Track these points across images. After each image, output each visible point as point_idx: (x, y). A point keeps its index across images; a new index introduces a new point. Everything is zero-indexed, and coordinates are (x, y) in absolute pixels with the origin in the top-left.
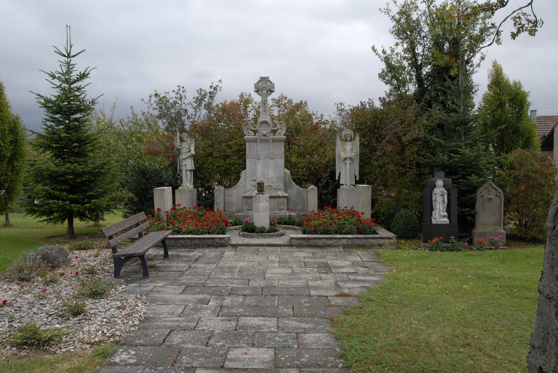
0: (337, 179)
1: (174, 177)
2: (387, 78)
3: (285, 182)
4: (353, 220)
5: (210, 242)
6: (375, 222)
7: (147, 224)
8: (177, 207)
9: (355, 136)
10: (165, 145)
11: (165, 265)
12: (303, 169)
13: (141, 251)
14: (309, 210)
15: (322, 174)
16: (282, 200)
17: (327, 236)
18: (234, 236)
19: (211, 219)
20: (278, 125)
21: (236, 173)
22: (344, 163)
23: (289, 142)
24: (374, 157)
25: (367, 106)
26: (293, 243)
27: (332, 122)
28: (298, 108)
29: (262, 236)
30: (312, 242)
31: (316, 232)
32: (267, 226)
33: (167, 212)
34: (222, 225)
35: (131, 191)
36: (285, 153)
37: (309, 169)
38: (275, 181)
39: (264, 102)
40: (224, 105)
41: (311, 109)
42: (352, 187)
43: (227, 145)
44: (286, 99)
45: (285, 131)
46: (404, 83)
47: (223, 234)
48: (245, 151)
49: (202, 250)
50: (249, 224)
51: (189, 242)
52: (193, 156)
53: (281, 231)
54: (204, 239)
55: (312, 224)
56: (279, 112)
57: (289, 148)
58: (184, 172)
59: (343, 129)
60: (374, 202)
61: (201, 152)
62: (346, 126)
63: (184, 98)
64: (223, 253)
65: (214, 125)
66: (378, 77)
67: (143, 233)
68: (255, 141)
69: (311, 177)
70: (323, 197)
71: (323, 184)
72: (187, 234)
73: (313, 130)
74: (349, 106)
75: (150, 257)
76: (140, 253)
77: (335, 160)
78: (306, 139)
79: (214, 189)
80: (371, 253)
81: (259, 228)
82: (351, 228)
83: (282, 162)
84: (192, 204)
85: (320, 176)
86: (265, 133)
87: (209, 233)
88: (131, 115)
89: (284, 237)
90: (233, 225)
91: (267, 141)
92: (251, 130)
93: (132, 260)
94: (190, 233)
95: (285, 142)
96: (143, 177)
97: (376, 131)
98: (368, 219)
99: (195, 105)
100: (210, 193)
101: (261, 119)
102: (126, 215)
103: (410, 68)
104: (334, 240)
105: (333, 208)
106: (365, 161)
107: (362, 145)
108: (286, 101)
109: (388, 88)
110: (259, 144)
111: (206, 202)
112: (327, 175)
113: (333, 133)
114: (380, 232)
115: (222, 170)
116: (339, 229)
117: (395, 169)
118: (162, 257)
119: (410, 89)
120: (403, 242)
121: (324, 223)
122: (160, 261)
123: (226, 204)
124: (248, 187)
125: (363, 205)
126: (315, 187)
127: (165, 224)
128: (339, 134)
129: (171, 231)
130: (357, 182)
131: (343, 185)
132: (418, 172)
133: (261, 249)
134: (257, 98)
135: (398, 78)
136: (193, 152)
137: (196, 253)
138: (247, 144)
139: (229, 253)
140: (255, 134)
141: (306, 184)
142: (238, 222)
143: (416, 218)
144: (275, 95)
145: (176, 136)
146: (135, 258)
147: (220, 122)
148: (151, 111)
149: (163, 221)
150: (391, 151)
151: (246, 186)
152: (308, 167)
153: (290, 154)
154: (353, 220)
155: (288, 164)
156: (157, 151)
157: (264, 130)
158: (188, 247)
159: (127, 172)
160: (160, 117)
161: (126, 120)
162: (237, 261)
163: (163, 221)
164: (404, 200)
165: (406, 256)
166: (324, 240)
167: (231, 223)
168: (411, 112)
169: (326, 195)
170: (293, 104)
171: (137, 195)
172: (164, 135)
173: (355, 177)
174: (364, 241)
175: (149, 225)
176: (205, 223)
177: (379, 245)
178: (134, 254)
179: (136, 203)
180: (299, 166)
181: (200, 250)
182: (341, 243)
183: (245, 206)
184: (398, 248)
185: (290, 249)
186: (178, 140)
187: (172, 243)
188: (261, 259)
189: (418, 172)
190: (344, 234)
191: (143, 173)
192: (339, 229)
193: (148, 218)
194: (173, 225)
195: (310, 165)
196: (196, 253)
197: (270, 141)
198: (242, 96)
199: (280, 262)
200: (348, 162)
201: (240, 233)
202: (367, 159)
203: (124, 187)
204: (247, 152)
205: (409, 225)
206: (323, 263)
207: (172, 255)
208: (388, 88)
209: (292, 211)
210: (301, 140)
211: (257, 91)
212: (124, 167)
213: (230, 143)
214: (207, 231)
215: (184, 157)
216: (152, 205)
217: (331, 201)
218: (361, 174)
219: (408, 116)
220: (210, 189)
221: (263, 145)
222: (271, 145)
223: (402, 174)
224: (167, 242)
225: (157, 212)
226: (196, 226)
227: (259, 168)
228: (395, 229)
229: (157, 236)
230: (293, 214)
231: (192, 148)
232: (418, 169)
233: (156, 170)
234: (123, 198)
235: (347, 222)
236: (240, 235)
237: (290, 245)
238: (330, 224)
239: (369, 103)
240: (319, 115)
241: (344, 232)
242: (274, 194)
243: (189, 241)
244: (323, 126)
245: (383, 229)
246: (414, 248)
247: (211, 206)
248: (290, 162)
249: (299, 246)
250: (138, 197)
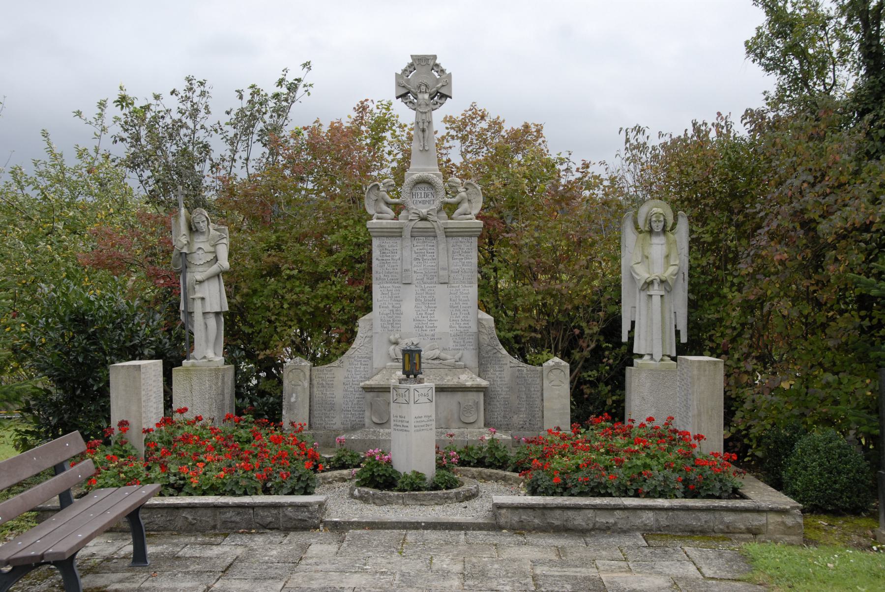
0: (625, 338)
1: (169, 331)
2: (769, 54)
3: (479, 348)
4: (672, 457)
5: (268, 517)
6: (736, 463)
7: (87, 466)
8: (177, 417)
9: (676, 218)
10: (146, 241)
11: (136, 586)
12: (530, 311)
13: (63, 547)
14: (546, 427)
15: (584, 324)
16: (472, 397)
17: (598, 501)
18: (337, 499)
19: (273, 450)
20: (461, 189)
21: (345, 323)
22: (643, 295)
23: (490, 239)
24: (730, 278)
25: (713, 135)
26: (502, 521)
27: (613, 180)
28: (519, 143)
29: (416, 499)
30: (556, 518)
31: (565, 490)
32: (429, 470)
33: (148, 431)
34: (303, 468)
35: (42, 370)
36: (480, 265)
37: (545, 310)
38: (451, 345)
39: (423, 127)
40: (314, 132)
41: (554, 146)
42: (668, 361)
43: (322, 246)
44: (483, 118)
45: (480, 205)
46: (822, 64)
47: (306, 493)
48: (370, 263)
49: (245, 539)
50: (379, 465)
51: (207, 518)
52: (224, 273)
53: (469, 485)
54: (252, 507)
55: (554, 465)
56: (463, 154)
57: (492, 253)
58: (198, 318)
59: (643, 201)
60: (731, 406)
61: (249, 264)
62: (650, 192)
63: (202, 114)
64: (305, 548)
65: (284, 188)
66: (744, 50)
67: (74, 493)
68: (396, 234)
69: (553, 332)
70: (587, 390)
71: (586, 353)
72: (204, 493)
73: (558, 202)
74: (661, 134)
75: (92, 562)
76: (63, 554)
77: (618, 287)
78: (538, 228)
79: (281, 365)
80: (728, 554)
81: (406, 476)
82: (666, 479)
83: (473, 292)
84: (221, 408)
85: (577, 331)
86: (424, 211)
87: (266, 491)
88: (46, 158)
89: (475, 503)
90: (333, 468)
91: (429, 234)
92: (388, 204)
93: (34, 573)
94: (213, 490)
95: (481, 237)
96: (79, 332)
97: (736, 205)
98: (716, 455)
99: (231, 132)
100: (270, 376)
101: (414, 173)
102: (25, 441)
103: (843, 20)
104: (618, 513)
105: (613, 421)
106: (702, 292)
107: (695, 242)
108: (484, 125)
109: (772, 82)
110: (408, 242)
111: (258, 401)
112: (596, 329)
113: (614, 209)
114: (750, 494)
115: (305, 313)
116: (632, 480)
117: (795, 314)
118: (127, 563)
119: (840, 81)
120: (823, 522)
121: (589, 463)
122: (120, 575)
123: (316, 407)
124: (378, 361)
125: (699, 415)
126: (564, 363)
127: (140, 466)
128: (631, 213)
129: (156, 486)
130: (682, 349)
131: (641, 356)
132: (866, 323)
133: (411, 536)
134: (404, 114)
135: (804, 52)
136: (224, 263)
137: (227, 549)
138: (375, 242)
139: (320, 547)
140: (398, 213)
141: (539, 353)
142: (347, 459)
143: (861, 454)
144: (453, 108)
145: (177, 217)
146: (47, 567)
147: (302, 180)
148: (106, 144)
149: (136, 458)
150: (782, 262)
151: (370, 358)
152: (544, 305)
153: (495, 270)
154: (672, 457)
155: (490, 298)
156: (120, 259)
157: (422, 204)
158: (203, 532)
159: (31, 319)
160: (133, 163)
161: (29, 171)
162: (342, 572)
163: (136, 458)
164: (823, 401)
165: (836, 569)
166: (590, 513)
167: (328, 461)
168: (841, 148)
169: (593, 384)
170: (503, 133)
171: (60, 382)
172: (142, 216)
173: (678, 333)
174: (704, 517)
175: (92, 469)
176: (254, 461)
177: (749, 531)
178: (42, 556)
179: (55, 405)
180: (519, 302)
181: (238, 540)
182: (638, 522)
183: (367, 414)
184: (808, 541)
185: (492, 538)
186: (184, 229)
187: (159, 519)
188: (412, 565)
189: (866, 323)
190: (648, 495)
191: (79, 320)
192: (632, 480)
193: (92, 449)
194: (164, 467)
195: (550, 301)
196: (227, 549)
197: (440, 233)
198: (362, 108)
199: (464, 576)
200: (656, 291)
201: (352, 489)
202: (711, 283)
203: (21, 361)
204: (375, 263)
205: (839, 473)
206: (586, 579)
207: (157, 557)
208: (772, 82)
209: (498, 428)
210: (525, 232)
211: (403, 96)
212: (23, 302)
213: (329, 239)
214: (259, 486)
215: (199, 277)
216: (106, 411)
217: (609, 402)
218: (693, 326)
219: (835, 162)
220: (271, 367)
221: (420, 245)
222: (442, 246)
223: (813, 328)
224: (144, 518)
225: (117, 431)
226: (230, 469)
227: (409, 308)
228: (798, 485)
229: (117, 501)
230: (502, 436)
231: (223, 252)
232: (863, 313)
233: (119, 313)
234: (19, 393)
235: (653, 463)
236: (352, 496)
237: (494, 527)
238: (606, 468)
239: (718, 126)
240: (576, 162)
241: (646, 489)
242: (450, 380)
243: (209, 512)
244: (587, 193)
245: (761, 484)
246: (859, 546)
247: (271, 413)
248: (495, 291)
249: (520, 529)
250: (64, 388)
